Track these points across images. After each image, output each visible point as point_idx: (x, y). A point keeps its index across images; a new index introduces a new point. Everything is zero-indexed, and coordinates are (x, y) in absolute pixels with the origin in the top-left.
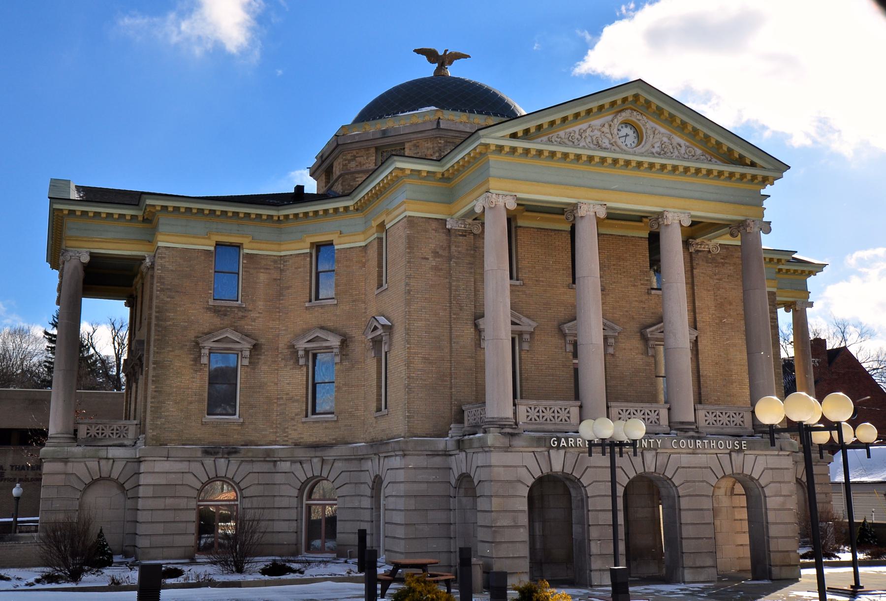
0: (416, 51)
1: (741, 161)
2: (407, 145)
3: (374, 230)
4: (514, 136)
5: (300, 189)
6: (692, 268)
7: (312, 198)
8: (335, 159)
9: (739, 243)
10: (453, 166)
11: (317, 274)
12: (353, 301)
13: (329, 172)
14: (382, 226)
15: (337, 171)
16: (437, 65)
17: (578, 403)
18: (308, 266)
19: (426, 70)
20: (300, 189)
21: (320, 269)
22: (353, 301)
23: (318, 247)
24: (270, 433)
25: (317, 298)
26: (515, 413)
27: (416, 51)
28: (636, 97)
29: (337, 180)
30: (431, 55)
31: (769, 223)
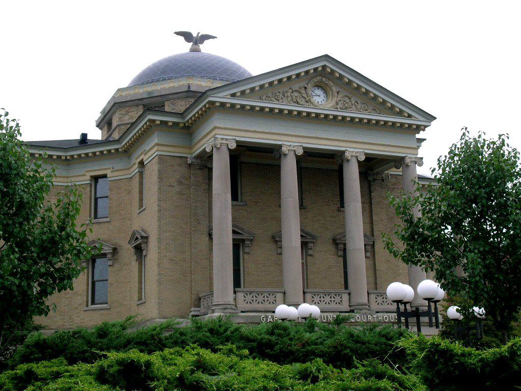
0: (175, 33)
1: (391, 110)
2: (166, 103)
3: (136, 166)
4: (233, 95)
5: (84, 136)
6: (301, 182)
7: (96, 143)
8: (114, 113)
9: (401, 174)
10: (194, 115)
11: (96, 199)
12: (122, 219)
13: (109, 124)
14: (142, 163)
15: (115, 123)
16: (192, 43)
17: (347, 291)
18: (89, 194)
19: (183, 47)
20: (84, 136)
21: (98, 196)
22: (122, 219)
23: (96, 179)
24: (60, 319)
25: (96, 217)
26: (235, 299)
27: (175, 33)
28: (324, 67)
29: (114, 130)
30: (187, 36)
31: (422, 158)
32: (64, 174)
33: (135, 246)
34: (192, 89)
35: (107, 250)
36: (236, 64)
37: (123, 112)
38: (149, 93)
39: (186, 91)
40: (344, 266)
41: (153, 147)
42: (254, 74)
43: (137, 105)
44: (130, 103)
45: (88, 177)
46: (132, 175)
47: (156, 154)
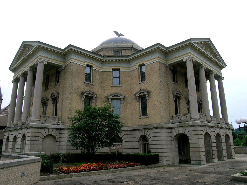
2: (123, 51)
19: (115, 36)
23: (141, 66)
30: (117, 33)
32: (101, 67)
33: (42, 102)
34: (133, 47)
35: (121, 97)
36: (136, 44)
37: (105, 51)
38: (117, 46)
39: (131, 47)
40: (198, 109)
41: (157, 57)
42: (144, 48)
43: (111, 50)
44: (109, 49)
45: (137, 66)
46: (130, 70)
47: (158, 60)
